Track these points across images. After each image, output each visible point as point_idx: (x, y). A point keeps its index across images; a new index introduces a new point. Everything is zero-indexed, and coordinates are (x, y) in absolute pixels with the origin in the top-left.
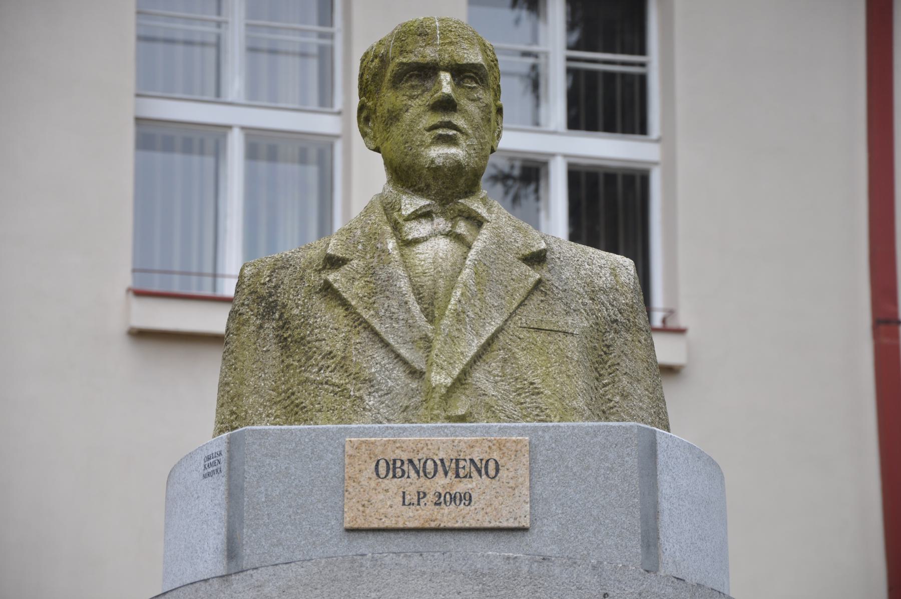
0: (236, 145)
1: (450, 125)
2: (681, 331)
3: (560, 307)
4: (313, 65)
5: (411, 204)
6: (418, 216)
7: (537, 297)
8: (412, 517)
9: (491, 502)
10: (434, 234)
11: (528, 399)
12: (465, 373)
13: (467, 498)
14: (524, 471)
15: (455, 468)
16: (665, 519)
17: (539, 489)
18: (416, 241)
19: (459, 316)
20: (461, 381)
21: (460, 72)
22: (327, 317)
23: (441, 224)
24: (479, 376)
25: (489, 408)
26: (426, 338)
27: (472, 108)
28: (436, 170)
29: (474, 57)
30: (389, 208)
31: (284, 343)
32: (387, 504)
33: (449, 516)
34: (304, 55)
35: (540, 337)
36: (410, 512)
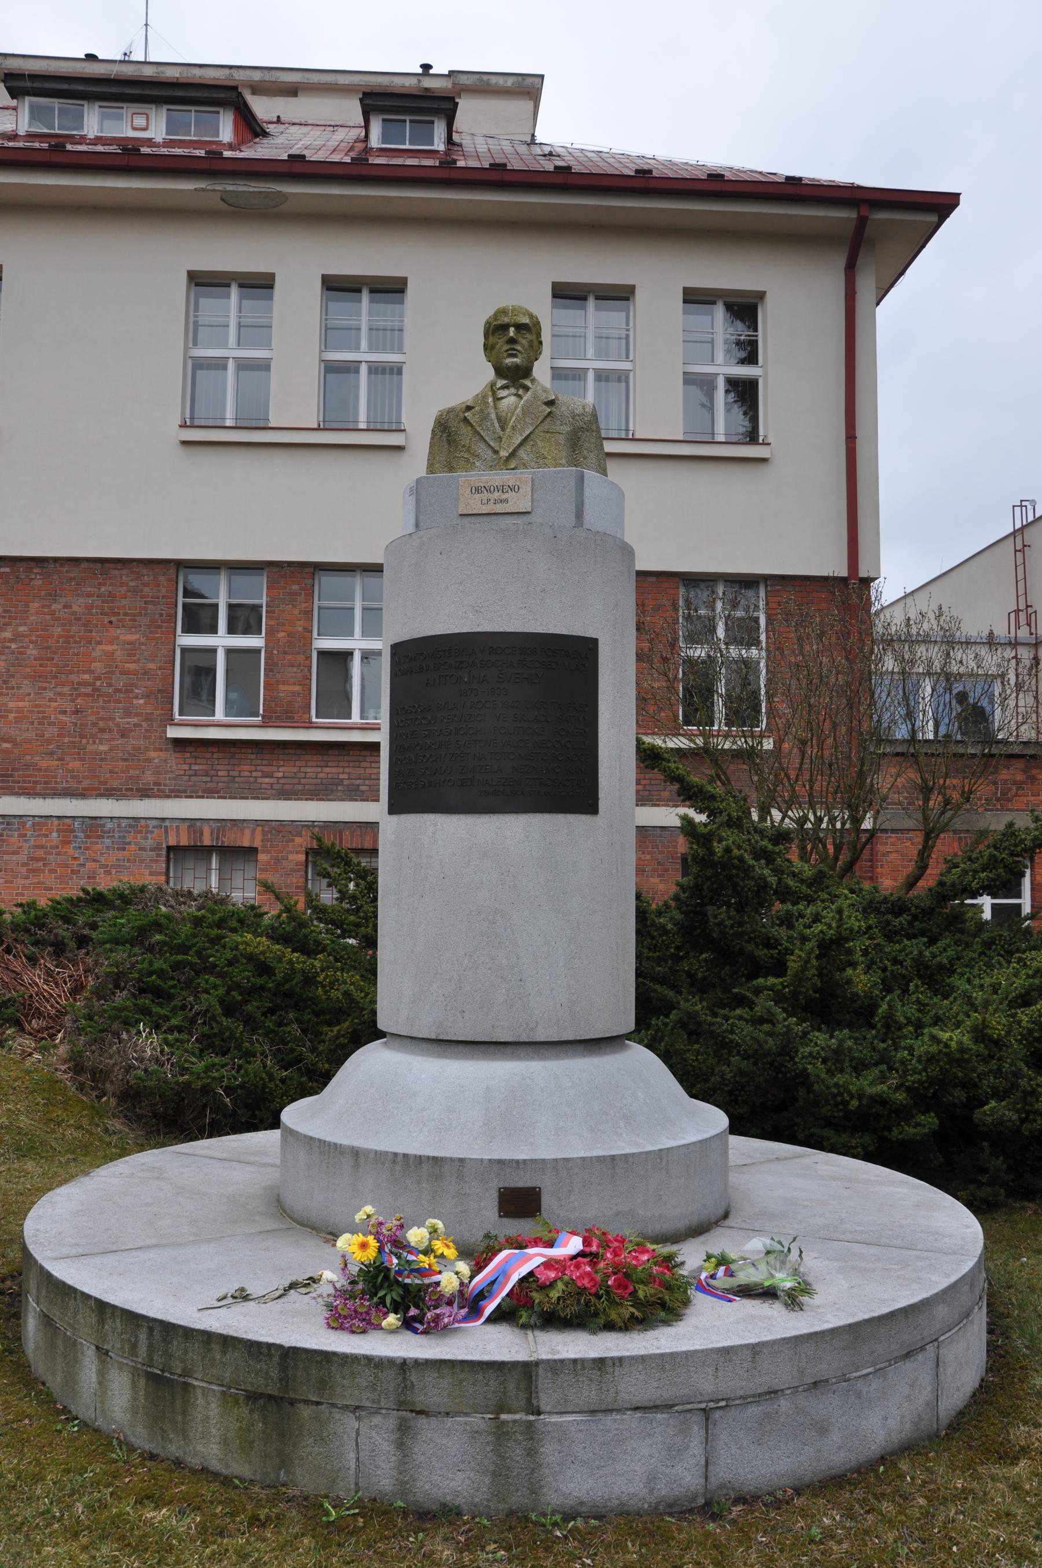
0: (591, 375)
1: (514, 349)
2: (769, 444)
3: (558, 422)
4: (624, 341)
5: (501, 383)
6: (503, 388)
7: (549, 419)
8: (485, 509)
9: (519, 502)
10: (509, 395)
11: (541, 460)
12: (515, 451)
13: (506, 501)
14: (529, 489)
15: (502, 489)
16: (586, 507)
17: (535, 496)
18: (502, 398)
19: (513, 428)
20: (513, 454)
21: (519, 327)
22: (465, 430)
23: (513, 390)
24: (521, 453)
25: (524, 465)
26: (500, 438)
27: (524, 341)
28: (508, 368)
29: (525, 320)
30: (493, 385)
31: (449, 442)
32: (475, 504)
33: (500, 508)
34: (620, 338)
35: (548, 435)
36: (484, 507)
